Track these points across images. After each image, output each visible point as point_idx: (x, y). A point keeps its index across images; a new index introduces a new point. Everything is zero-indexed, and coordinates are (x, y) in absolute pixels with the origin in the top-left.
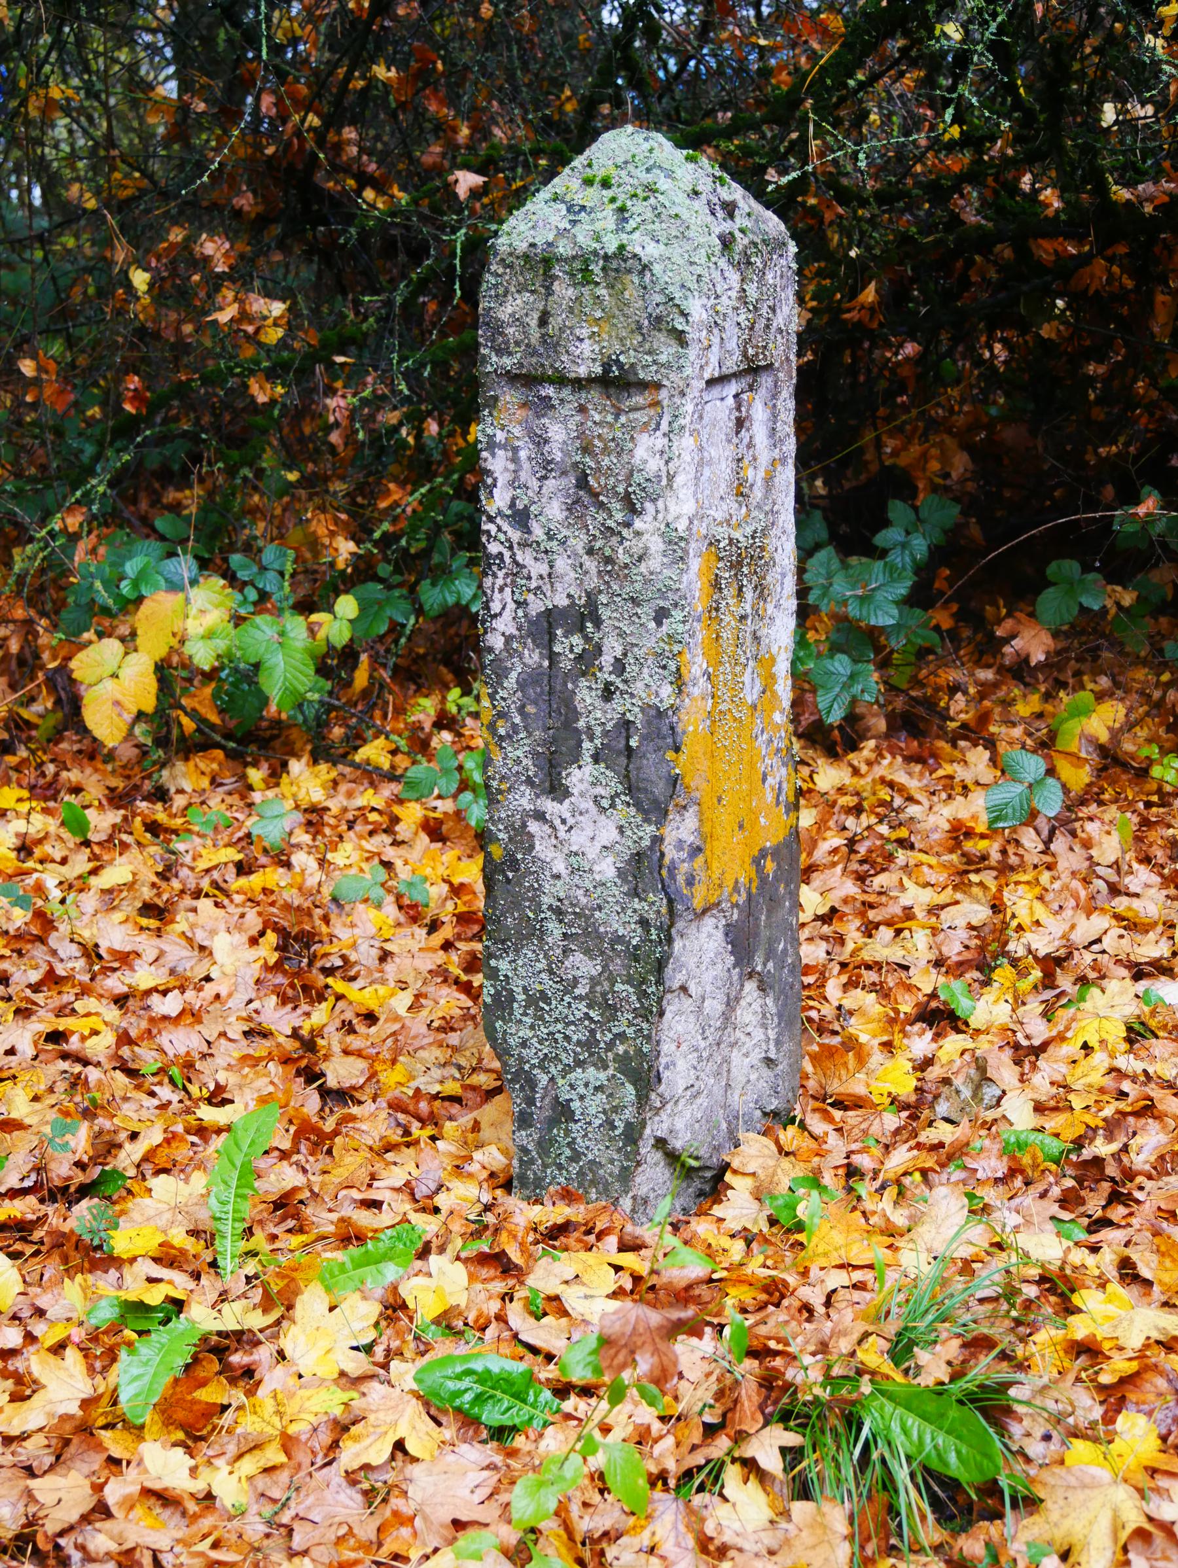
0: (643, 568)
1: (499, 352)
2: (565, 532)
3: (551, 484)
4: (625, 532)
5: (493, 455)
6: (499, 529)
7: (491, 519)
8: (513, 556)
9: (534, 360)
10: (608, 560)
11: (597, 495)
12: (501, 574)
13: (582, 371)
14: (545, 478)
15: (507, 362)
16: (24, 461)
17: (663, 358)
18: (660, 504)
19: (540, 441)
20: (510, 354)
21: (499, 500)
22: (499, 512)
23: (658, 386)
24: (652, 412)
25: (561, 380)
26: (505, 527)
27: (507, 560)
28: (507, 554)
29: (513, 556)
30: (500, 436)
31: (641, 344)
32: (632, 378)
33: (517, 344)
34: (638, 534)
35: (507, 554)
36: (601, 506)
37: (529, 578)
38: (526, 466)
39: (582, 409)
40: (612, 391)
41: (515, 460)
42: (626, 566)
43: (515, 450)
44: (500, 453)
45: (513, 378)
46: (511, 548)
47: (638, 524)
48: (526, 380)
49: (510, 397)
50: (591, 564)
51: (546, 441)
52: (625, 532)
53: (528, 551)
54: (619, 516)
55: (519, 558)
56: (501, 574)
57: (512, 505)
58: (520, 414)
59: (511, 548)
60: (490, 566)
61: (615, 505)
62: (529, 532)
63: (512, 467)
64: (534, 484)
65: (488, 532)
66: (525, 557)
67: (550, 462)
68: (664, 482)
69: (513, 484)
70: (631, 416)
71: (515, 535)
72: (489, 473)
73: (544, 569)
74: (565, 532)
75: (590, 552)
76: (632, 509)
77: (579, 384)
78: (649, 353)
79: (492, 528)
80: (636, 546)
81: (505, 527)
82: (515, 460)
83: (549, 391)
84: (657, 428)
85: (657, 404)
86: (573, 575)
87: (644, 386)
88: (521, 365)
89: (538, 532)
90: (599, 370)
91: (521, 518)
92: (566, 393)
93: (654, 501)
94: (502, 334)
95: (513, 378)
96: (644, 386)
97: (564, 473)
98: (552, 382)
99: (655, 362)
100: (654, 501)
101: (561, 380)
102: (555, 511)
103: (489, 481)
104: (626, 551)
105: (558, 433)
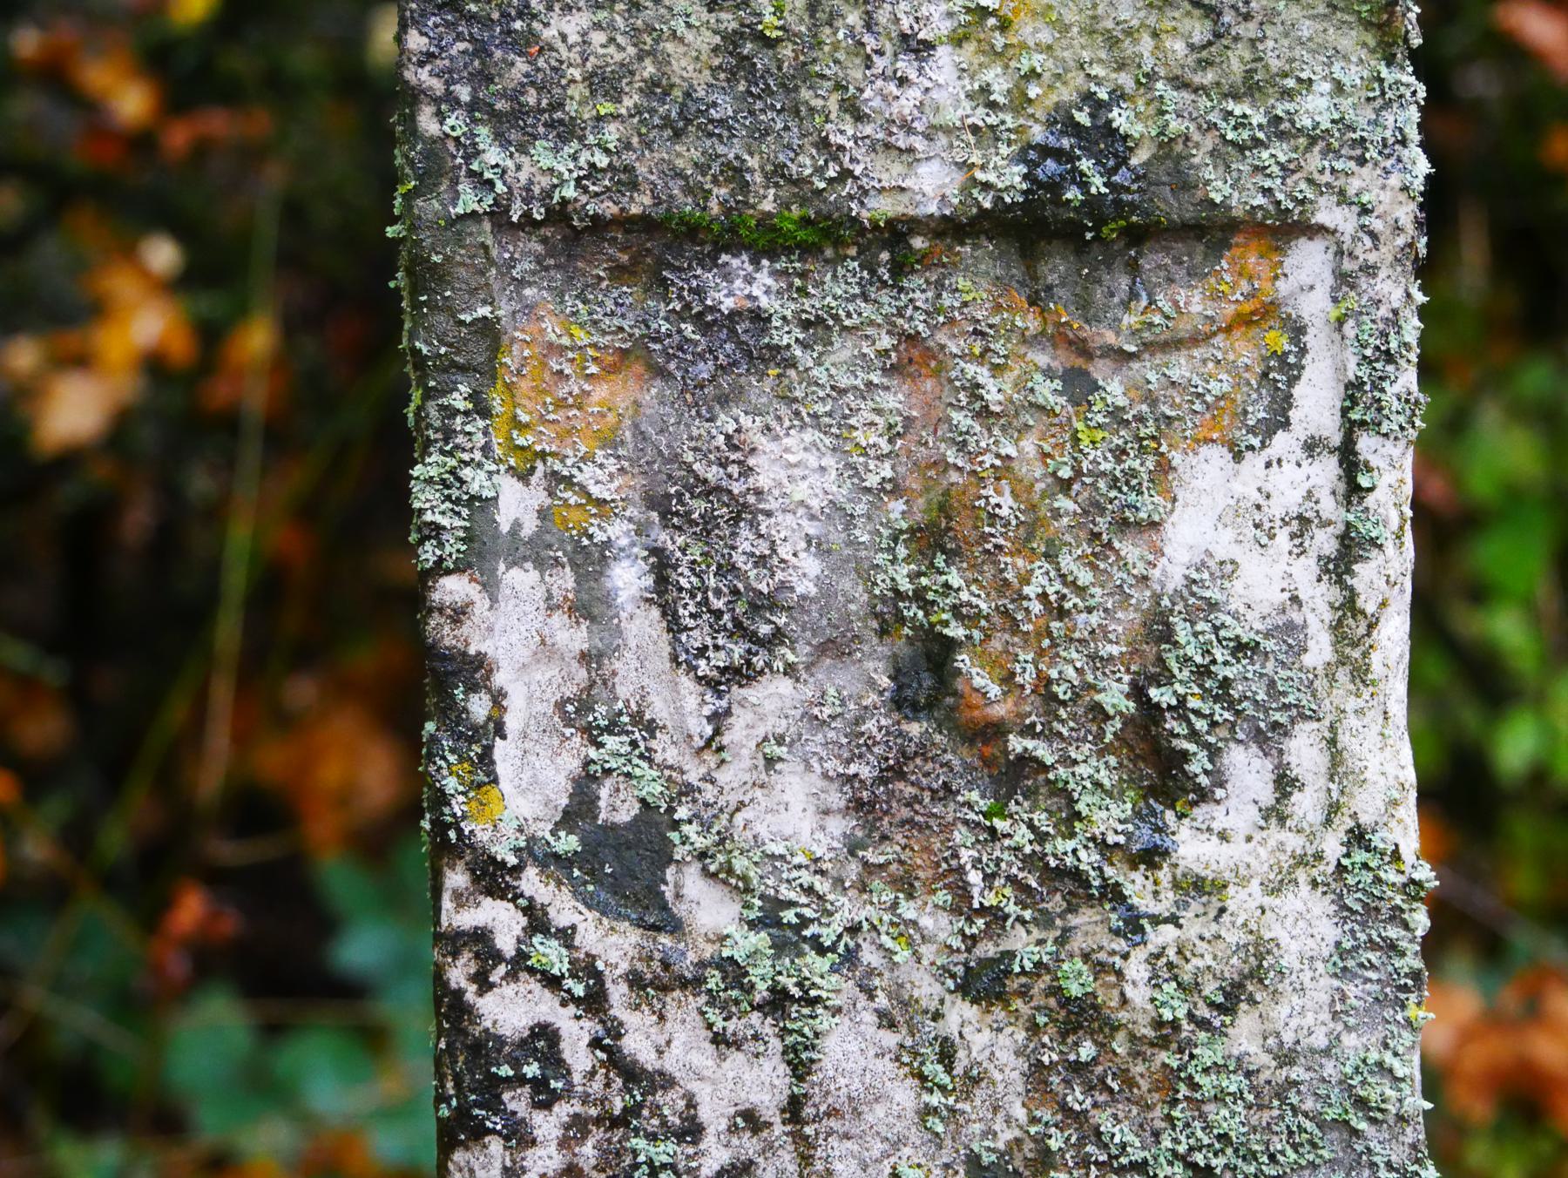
0: (1244, 1036)
1: (512, 124)
2: (848, 908)
3: (771, 700)
4: (1136, 886)
5: (490, 587)
6: (537, 920)
7: (493, 878)
8: (608, 1046)
9: (687, 154)
10: (1080, 1016)
11: (995, 731)
12: (547, 1125)
13: (932, 185)
14: (741, 674)
15: (548, 167)
16: (741, 884)
17: (1315, 108)
18: (1304, 751)
19: (699, 508)
20: (566, 131)
21: (523, 790)
22: (532, 852)
23: (1284, 228)
24: (1245, 352)
25: (819, 234)
26: (564, 909)
27: (578, 1056)
28: (576, 1034)
29: (608, 1046)
30: (517, 505)
31: (1204, 56)
32: (1170, 207)
33: (604, 83)
34: (1197, 886)
35: (576, 1034)
36: (1014, 777)
37: (691, 1130)
38: (642, 628)
39: (912, 357)
40: (1055, 268)
41: (589, 606)
42: (1165, 1033)
43: (591, 561)
44: (520, 580)
45: (568, 234)
46: (594, 1003)
47: (1192, 848)
48: (658, 244)
49: (547, 324)
50: (991, 1041)
51: (743, 512)
52: (1136, 886)
53: (685, 1012)
54: (1109, 817)
55: (638, 1044)
56: (547, 1125)
57: (579, 808)
58: (615, 397)
59: (594, 1003)
60: (492, 1090)
61: (1091, 770)
62: (675, 926)
63: (573, 637)
64: (682, 705)
65: (481, 938)
66: (667, 1039)
67: (763, 604)
68: (1320, 651)
69: (580, 714)
70: (1148, 371)
71: (614, 945)
72: (475, 670)
73: (761, 1081)
74: (848, 908)
75: (984, 983)
76: (1164, 774)
77: (895, 246)
78: (1250, 88)
79: (502, 921)
80: (1209, 945)
81: (564, 909)
82: (589, 606)
83: (747, 285)
84: (1279, 420)
85: (1263, 313)
86: (905, 1095)
87: (1213, 232)
88: (628, 181)
89: (710, 912)
90: (1010, 177)
91: (625, 861)
92: (835, 288)
93: (1268, 738)
94: (525, 43)
95: (568, 234)
96: (1213, 232)
97: (835, 648)
98: (767, 242)
99: (1279, 128)
100: (1268, 738)
101: (819, 234)
102: (795, 818)
103: (479, 707)
104: (1164, 969)
105: (799, 478)
